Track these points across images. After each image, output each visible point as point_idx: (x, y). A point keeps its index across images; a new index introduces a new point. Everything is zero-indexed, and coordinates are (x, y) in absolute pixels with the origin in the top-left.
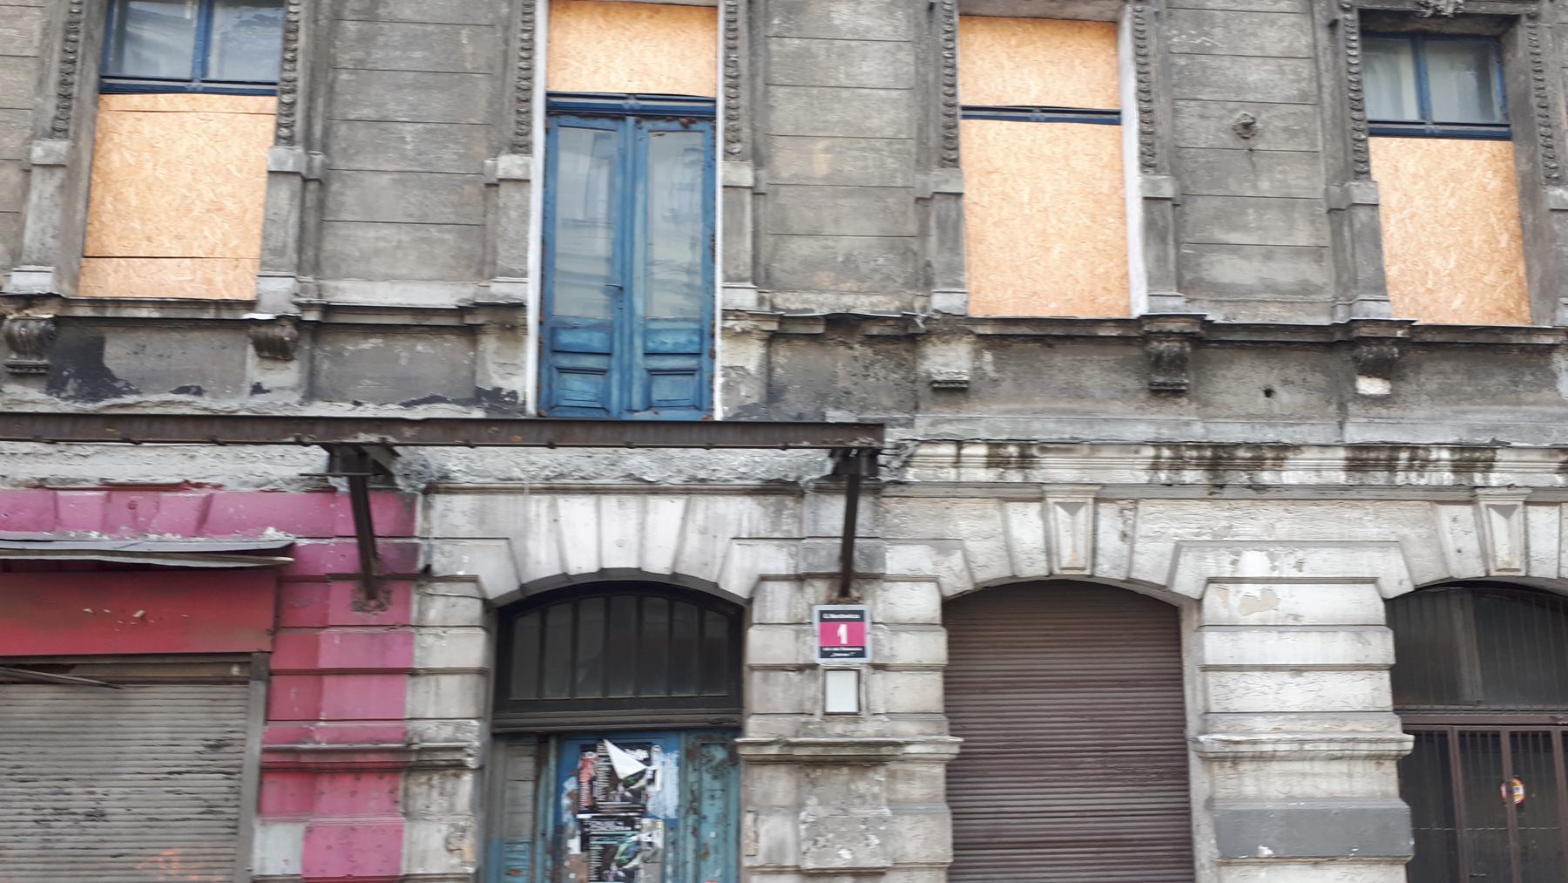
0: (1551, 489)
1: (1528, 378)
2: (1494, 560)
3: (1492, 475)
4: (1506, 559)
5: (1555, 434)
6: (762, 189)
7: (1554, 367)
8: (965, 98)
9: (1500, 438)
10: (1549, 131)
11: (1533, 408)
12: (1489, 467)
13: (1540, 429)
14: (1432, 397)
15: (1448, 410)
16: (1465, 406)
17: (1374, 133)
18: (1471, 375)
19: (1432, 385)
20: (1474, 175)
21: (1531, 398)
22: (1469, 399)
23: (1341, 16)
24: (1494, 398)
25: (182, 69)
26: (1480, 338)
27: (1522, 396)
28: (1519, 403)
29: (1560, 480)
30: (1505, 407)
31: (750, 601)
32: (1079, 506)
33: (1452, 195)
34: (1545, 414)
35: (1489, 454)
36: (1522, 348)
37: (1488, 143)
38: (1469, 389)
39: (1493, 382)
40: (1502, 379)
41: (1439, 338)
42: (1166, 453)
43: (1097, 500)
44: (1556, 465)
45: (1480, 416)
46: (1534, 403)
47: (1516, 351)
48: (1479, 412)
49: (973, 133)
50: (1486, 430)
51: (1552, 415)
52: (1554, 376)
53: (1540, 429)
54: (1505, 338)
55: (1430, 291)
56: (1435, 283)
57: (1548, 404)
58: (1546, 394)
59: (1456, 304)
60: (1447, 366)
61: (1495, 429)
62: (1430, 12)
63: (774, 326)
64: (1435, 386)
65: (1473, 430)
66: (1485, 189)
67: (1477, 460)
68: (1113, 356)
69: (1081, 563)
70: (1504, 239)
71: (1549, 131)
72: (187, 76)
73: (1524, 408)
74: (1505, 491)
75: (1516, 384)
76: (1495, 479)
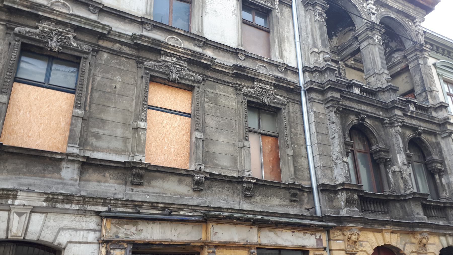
0: (40, 207)
1: (50, 169)
2: (11, 232)
3: (16, 201)
4: (15, 232)
5: (54, 188)
6: (85, 118)
7: (61, 166)
8: (150, 103)
9: (30, 188)
10: (81, 92)
11: (49, 179)
12: (15, 197)
13: (48, 186)
14: (8, 172)
15: (14, 177)
16: (21, 176)
17: (148, 108)
18: (27, 165)
19: (10, 168)
20: (58, 102)
21: (49, 176)
22: (24, 174)
23: (244, 101)
24: (35, 175)
25: (41, 79)
26: (32, 153)
27: (46, 175)
28: (44, 177)
29: (44, 204)
30: (38, 178)
31: (64, 248)
32: (23, 214)
33: (48, 107)
34: (53, 182)
35: (15, 193)
36: (50, 158)
37: (66, 94)
38: (25, 170)
39: (36, 169)
40: (40, 168)
41: (15, 151)
42: (51, 196)
43: (32, 212)
44: (43, 199)
45: (27, 180)
46: (50, 178)
47: (48, 159)
48: (26, 179)
49: (150, 112)
50: (26, 185)
51: (56, 182)
52: (61, 169)
53: (48, 186)
54: (42, 154)
55: (29, 137)
56: (32, 135)
57: (55, 178)
58: (56, 175)
59: (39, 142)
60: (18, 162)
61: (30, 185)
62: (49, 49)
63: (85, 160)
64: (11, 168)
65: (20, 184)
66: (61, 107)
67: (10, 195)
68: (282, 192)
69: (20, 234)
70: (63, 124)
71: (81, 92)
72: (43, 81)
73: (45, 179)
74: (22, 207)
75: (45, 170)
76: (17, 202)
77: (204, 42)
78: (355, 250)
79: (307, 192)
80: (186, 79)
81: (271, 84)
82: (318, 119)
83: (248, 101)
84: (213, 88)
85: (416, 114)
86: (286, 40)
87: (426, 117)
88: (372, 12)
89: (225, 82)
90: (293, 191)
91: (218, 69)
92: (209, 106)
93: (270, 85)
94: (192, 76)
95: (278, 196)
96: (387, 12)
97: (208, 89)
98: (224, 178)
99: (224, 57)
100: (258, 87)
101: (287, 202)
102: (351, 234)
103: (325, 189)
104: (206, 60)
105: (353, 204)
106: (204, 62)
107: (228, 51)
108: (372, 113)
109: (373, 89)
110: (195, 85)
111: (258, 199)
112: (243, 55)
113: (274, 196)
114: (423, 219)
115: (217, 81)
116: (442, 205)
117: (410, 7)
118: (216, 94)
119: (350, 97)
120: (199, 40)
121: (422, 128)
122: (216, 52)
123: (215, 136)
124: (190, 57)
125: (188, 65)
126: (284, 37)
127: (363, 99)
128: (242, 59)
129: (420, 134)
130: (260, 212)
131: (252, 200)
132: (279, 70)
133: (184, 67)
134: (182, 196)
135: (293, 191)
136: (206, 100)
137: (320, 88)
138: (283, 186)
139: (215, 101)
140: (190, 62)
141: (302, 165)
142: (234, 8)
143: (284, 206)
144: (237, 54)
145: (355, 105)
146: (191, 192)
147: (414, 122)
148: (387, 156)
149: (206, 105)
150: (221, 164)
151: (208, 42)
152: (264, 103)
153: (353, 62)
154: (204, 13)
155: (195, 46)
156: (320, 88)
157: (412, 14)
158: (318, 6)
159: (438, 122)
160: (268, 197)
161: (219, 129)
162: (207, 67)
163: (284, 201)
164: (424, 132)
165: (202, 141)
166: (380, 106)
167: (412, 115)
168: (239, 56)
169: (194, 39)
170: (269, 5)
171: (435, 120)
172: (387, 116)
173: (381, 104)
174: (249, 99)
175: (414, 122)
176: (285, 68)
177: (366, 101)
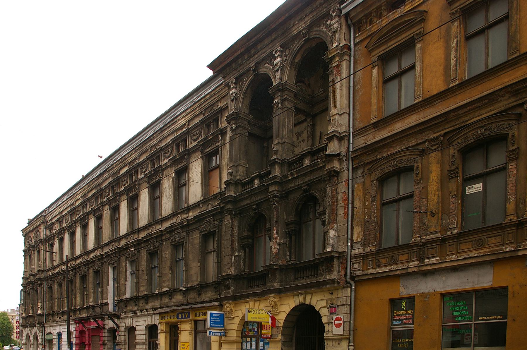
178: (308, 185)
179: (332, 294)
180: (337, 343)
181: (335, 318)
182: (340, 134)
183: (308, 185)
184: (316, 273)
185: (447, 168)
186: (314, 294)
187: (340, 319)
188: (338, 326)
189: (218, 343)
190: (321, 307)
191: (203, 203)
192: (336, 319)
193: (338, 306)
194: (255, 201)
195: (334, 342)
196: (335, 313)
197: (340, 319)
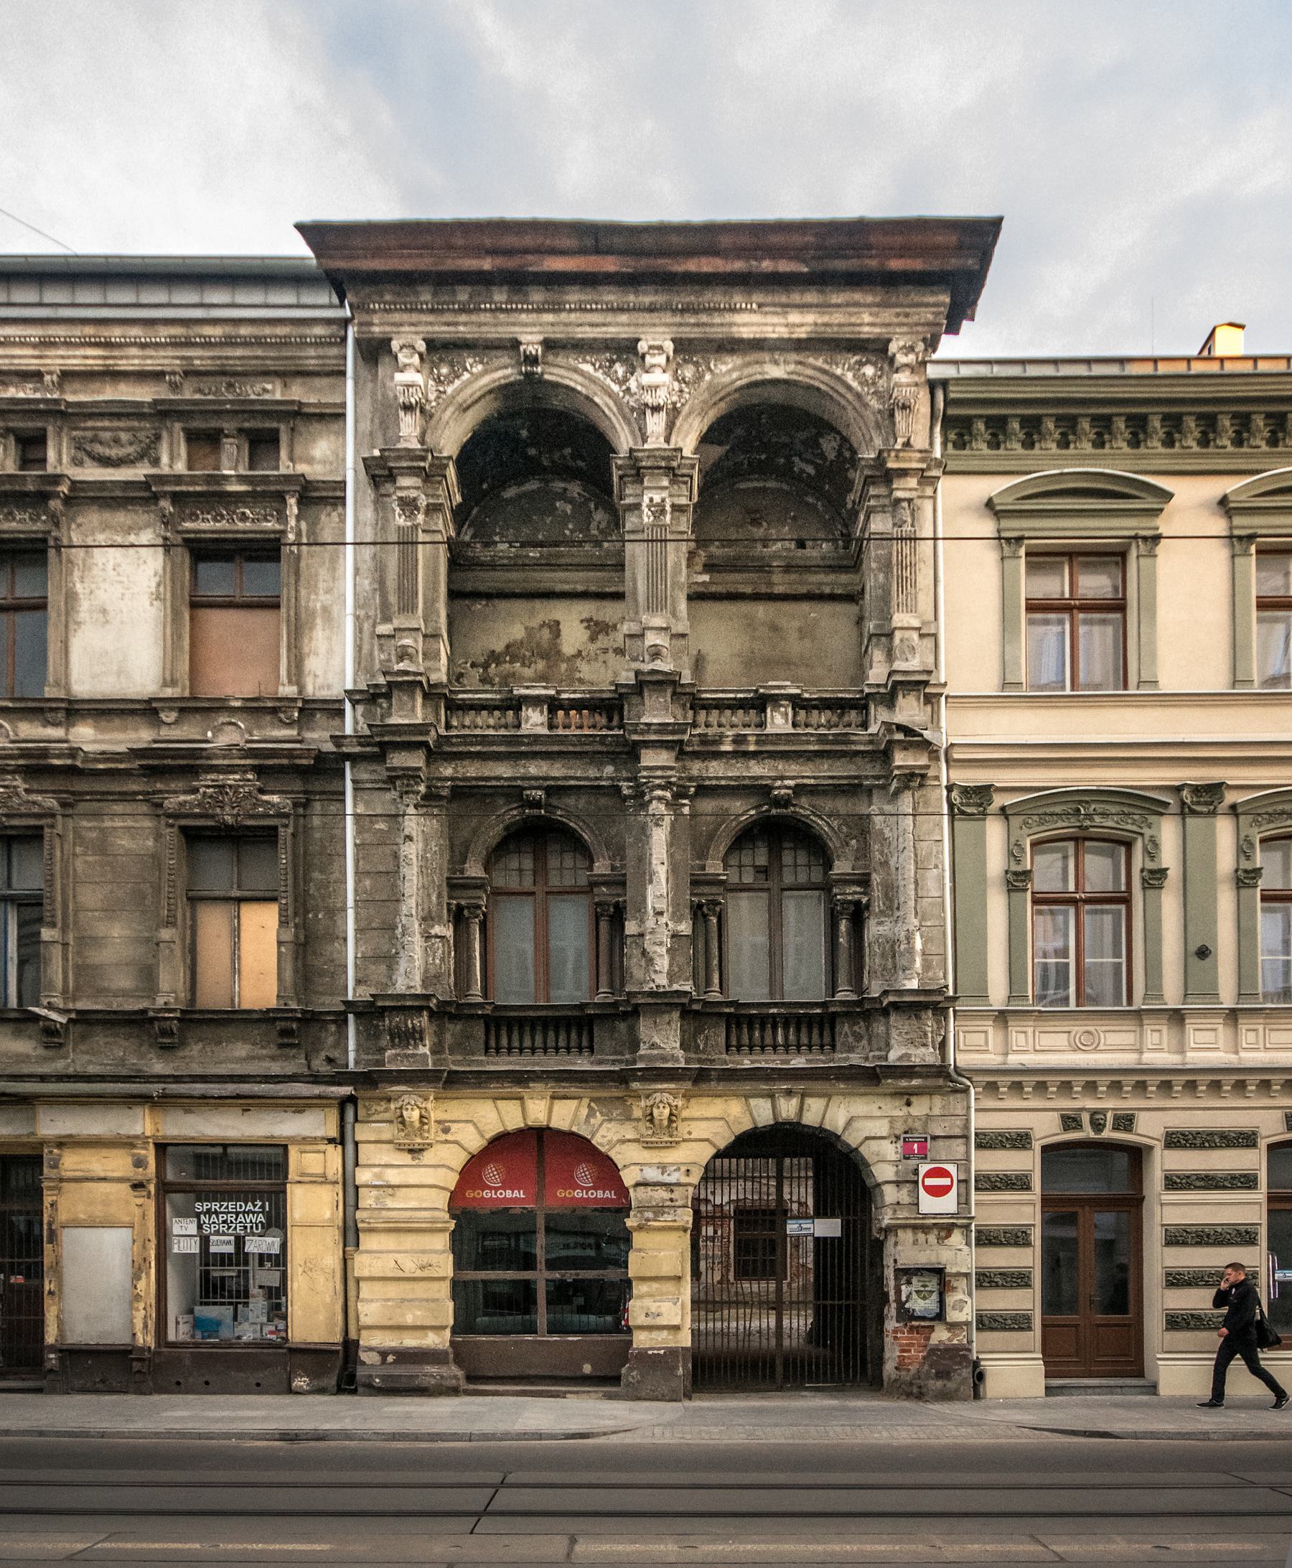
68: (255, 1032)
77: (67, 710)
78: (419, 1140)
79: (334, 1022)
80: (21, 816)
81: (244, 769)
82: (366, 835)
83: (183, 829)
84: (97, 815)
85: (757, 743)
86: (319, 621)
87: (808, 743)
88: (646, 405)
89: (125, 793)
90: (279, 1025)
91: (101, 766)
92: (86, 862)
93: (245, 772)
94: (34, 803)
95: (244, 1040)
96: (748, 364)
97: (85, 824)
98: (113, 1017)
99: (124, 729)
100: (208, 787)
101: (272, 1050)
102: (401, 1108)
103: (370, 1012)
104: (59, 757)
105: (415, 1039)
106: (56, 762)
107: (133, 712)
108: (565, 778)
109: (605, 696)
110: (42, 822)
111: (195, 1049)
112: (171, 709)
113: (238, 1040)
114: (674, 1058)
115: (104, 797)
116: (818, 1011)
117: (857, 304)
118: (102, 830)
119: (478, 748)
120: (51, 709)
121: (791, 783)
122: (103, 723)
123: (101, 929)
124: (21, 762)
125: (25, 781)
126: (313, 614)
127: (528, 744)
128: (168, 720)
129: (784, 802)
130: (174, 1076)
131: (181, 1054)
132: (281, 721)
133: (15, 787)
134: (24, 1058)
135: (279, 1025)
136: (78, 850)
137: (368, 749)
138: (256, 1016)
139: (101, 847)
140: (30, 772)
141: (332, 961)
142: (157, 579)
143: (260, 1058)
144: (155, 712)
145: (504, 770)
146: (41, 1051)
147: (757, 769)
148: (619, 895)
149: (79, 864)
150: (113, 986)
151: (77, 707)
152: (225, 823)
153: (706, 578)
154: (72, 626)
155: (44, 726)
156: (368, 749)
157: (867, 331)
158: (402, 475)
159: (869, 748)
160: (220, 1043)
161: (110, 910)
162: (72, 771)
163: (263, 1047)
164: (799, 790)
165: (60, 947)
166: (600, 748)
167: (743, 748)
168: (162, 716)
169: (41, 710)
170: (269, 525)
171: (853, 743)
172: (625, 774)
173: (602, 744)
174: (183, 822)
175: (757, 769)
176: (301, 710)
177: (537, 748)
178: (549, 791)
179: (909, 1104)
180: (932, 1238)
181: (924, 1169)
182: (885, 686)
183: (549, 791)
184: (827, 1039)
185: (445, 875)
186: (834, 1098)
187: (945, 1174)
188: (938, 1191)
189: (334, 1235)
190: (867, 1138)
191: (182, 710)
192: (930, 1174)
193: (934, 1138)
194: (545, 779)
195: (921, 1236)
196: (924, 1157)
197: (945, 1174)
